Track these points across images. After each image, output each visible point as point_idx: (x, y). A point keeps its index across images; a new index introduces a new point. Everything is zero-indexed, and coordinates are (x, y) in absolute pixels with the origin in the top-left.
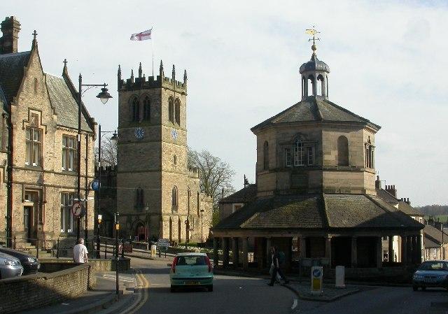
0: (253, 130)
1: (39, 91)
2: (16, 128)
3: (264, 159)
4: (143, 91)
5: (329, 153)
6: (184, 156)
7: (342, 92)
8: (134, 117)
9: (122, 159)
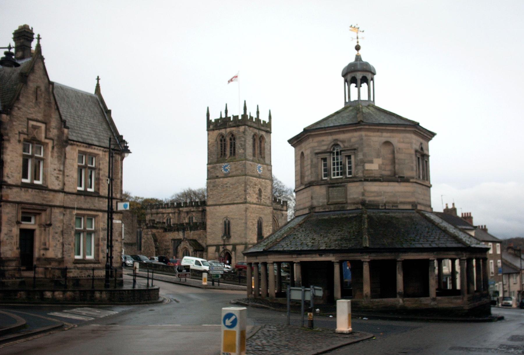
0: (290, 141)
1: (41, 100)
2: (9, 140)
3: (301, 173)
4: (228, 130)
5: (371, 162)
6: (269, 190)
7: (388, 95)
8: (222, 154)
9: (211, 193)
